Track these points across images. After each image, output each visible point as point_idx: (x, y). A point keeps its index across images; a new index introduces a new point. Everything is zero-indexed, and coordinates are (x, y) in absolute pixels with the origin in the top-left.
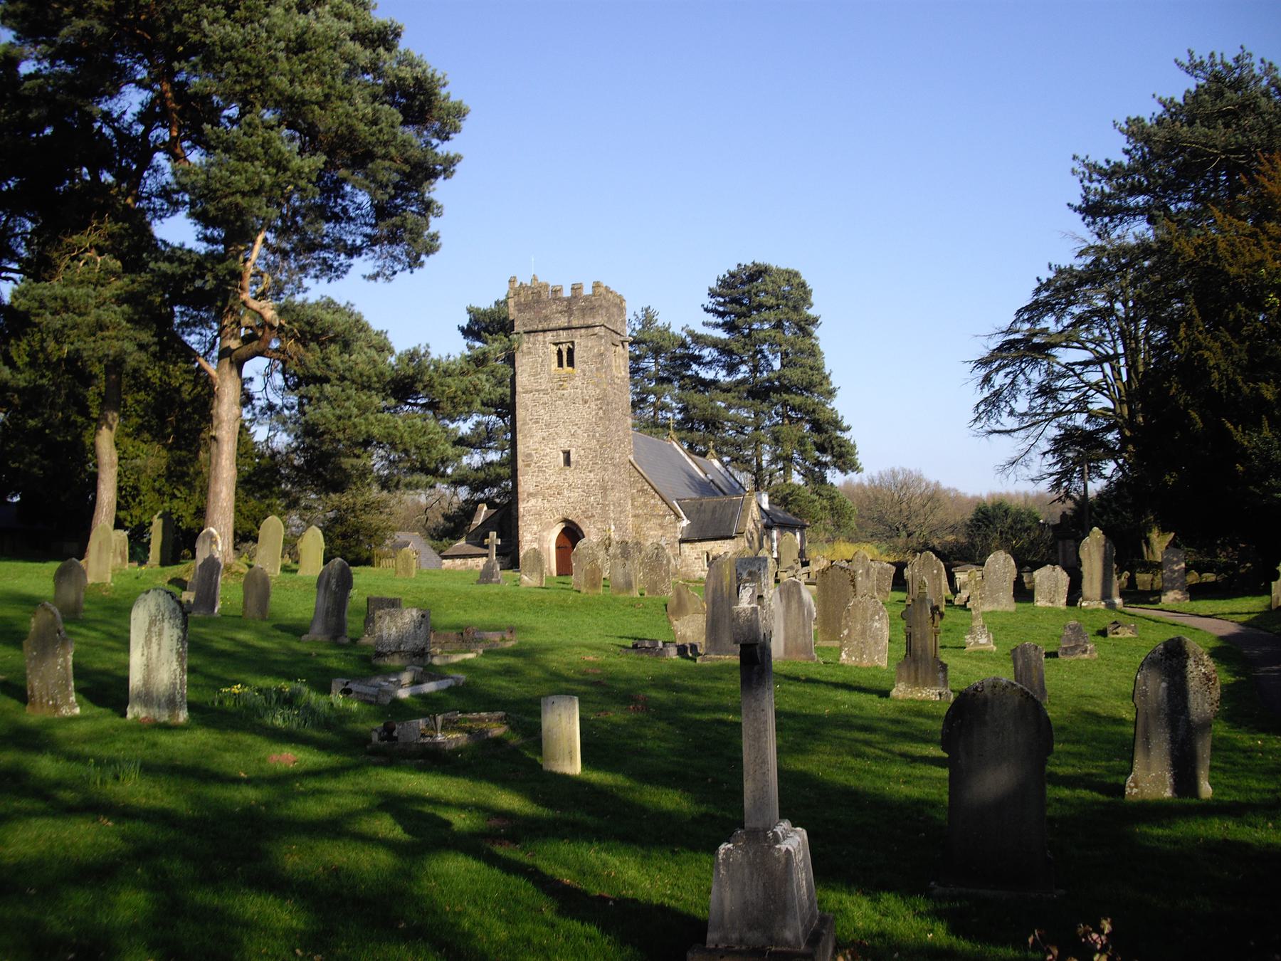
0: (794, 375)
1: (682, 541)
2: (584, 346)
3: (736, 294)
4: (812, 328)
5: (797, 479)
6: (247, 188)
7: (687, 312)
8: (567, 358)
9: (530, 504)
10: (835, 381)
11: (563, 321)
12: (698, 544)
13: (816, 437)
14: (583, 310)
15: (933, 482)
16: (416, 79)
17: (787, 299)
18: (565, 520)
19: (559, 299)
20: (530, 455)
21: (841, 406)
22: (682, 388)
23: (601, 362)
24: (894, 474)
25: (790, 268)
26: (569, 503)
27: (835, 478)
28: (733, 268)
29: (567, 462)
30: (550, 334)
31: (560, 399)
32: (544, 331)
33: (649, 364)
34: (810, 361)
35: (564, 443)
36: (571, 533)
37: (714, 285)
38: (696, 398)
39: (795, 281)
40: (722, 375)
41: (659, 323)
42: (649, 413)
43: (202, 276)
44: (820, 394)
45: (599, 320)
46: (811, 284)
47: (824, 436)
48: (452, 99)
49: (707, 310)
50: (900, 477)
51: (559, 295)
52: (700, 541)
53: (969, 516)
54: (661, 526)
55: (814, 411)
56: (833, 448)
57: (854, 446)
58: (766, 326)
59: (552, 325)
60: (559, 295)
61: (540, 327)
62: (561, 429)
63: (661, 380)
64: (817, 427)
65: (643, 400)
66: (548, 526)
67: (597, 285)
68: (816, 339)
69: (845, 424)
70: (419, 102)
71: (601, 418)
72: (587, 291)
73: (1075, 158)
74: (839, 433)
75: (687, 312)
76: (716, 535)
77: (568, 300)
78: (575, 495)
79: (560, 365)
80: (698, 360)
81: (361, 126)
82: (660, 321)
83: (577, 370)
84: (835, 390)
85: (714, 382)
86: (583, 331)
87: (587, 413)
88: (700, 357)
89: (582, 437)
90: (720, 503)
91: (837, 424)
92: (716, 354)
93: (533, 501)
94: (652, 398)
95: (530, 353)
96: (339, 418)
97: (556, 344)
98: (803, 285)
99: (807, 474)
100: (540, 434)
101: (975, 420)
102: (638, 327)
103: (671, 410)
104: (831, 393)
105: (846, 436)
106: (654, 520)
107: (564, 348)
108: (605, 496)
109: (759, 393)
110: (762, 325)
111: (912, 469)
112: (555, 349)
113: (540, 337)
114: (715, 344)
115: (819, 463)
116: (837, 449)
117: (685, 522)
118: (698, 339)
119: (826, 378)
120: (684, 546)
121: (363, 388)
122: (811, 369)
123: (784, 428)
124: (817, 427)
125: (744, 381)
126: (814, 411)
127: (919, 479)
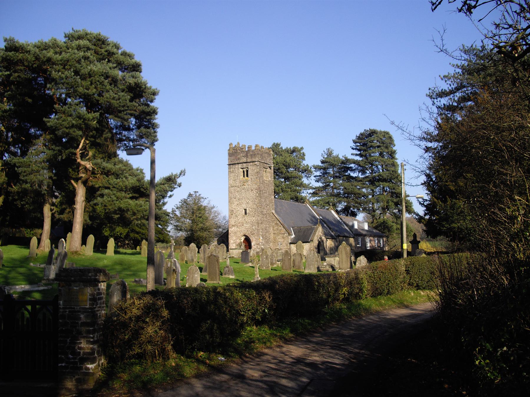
1: (291, 243)
2: (252, 169)
3: (363, 141)
6: (68, 126)
7: (345, 150)
8: (246, 174)
11: (244, 160)
16: (135, 83)
17: (383, 144)
18: (245, 235)
25: (386, 130)
26: (245, 229)
28: (362, 131)
29: (246, 213)
31: (243, 189)
32: (238, 164)
33: (331, 171)
35: (244, 206)
36: (248, 241)
39: (387, 136)
40: (361, 176)
41: (334, 154)
43: (61, 155)
45: (257, 159)
49: (353, 149)
54: (283, 238)
57: (412, 203)
59: (241, 161)
61: (237, 162)
62: (243, 201)
67: (256, 146)
68: (396, 159)
72: (253, 148)
73: (429, 89)
75: (345, 150)
77: (247, 152)
78: (248, 226)
79: (244, 177)
81: (112, 101)
82: (335, 154)
83: (249, 179)
87: (253, 194)
88: (351, 167)
89: (251, 203)
93: (233, 228)
96: (109, 201)
100: (236, 203)
102: (326, 156)
107: (245, 170)
108: (258, 227)
109: (373, 181)
112: (242, 170)
114: (354, 162)
120: (292, 245)
121: (120, 191)
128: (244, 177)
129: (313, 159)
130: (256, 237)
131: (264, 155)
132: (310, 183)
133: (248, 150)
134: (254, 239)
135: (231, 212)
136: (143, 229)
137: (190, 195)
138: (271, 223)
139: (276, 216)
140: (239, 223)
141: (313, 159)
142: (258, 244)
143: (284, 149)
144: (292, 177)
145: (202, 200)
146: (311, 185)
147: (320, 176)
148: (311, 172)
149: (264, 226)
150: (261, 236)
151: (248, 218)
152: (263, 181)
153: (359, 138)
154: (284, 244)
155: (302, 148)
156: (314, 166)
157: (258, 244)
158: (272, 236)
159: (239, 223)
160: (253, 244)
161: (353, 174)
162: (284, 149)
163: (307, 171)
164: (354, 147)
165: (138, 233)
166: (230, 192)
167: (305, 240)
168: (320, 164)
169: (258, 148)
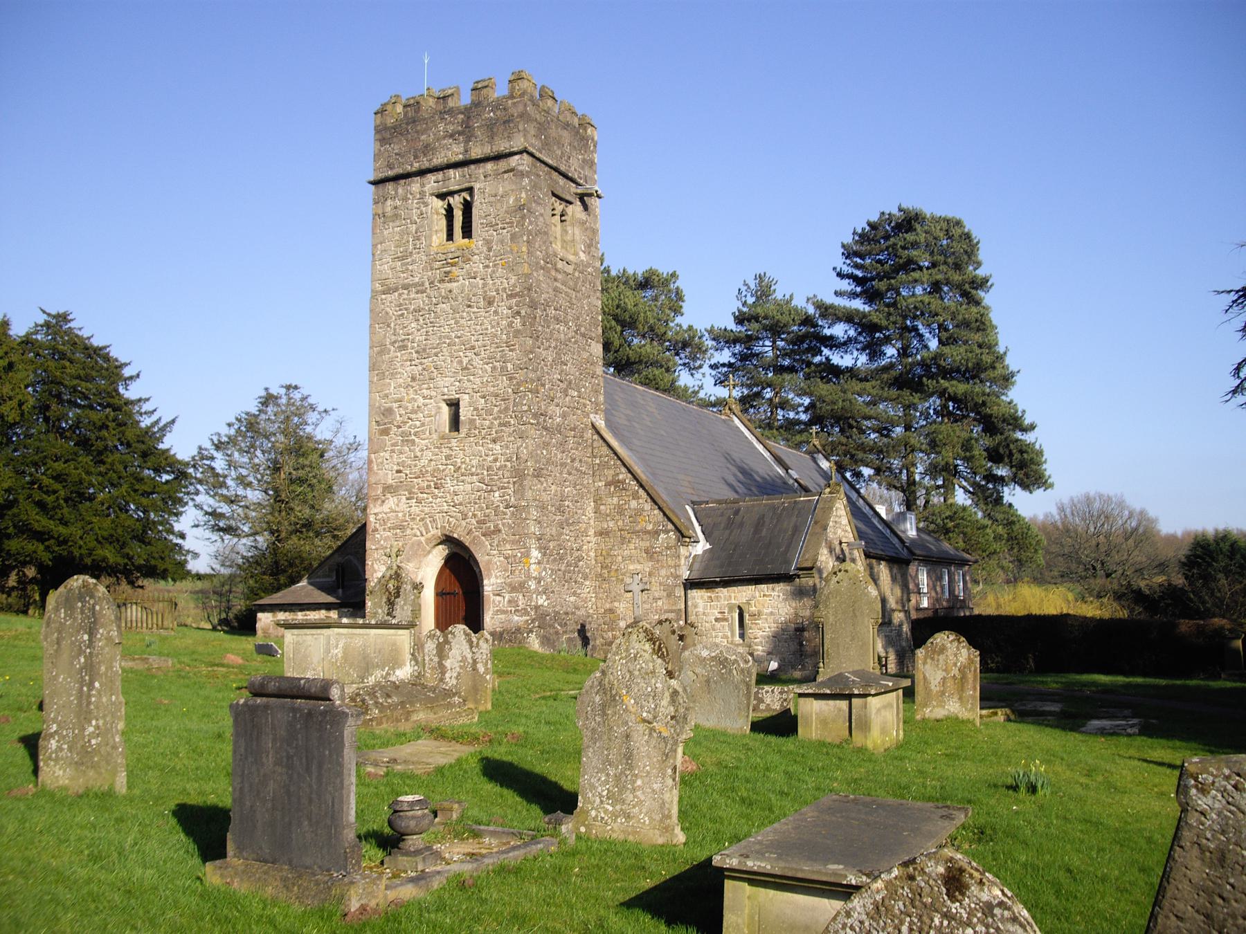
0: (955, 355)
1: (690, 584)
2: (493, 192)
4: (981, 293)
5: (961, 498)
7: (813, 278)
8: (463, 221)
9: (386, 508)
10: (1012, 362)
11: (455, 152)
12: (723, 592)
13: (987, 441)
14: (491, 127)
15: (1138, 510)
18: (448, 540)
19: (451, 112)
20: (389, 411)
21: (1022, 396)
22: (808, 377)
23: (521, 224)
24: (1088, 500)
25: (950, 215)
26: (453, 507)
27: (1014, 496)
28: (875, 218)
29: (455, 423)
30: (431, 178)
32: (422, 173)
33: (766, 348)
34: (978, 337)
35: (448, 385)
37: (848, 239)
38: (823, 389)
39: (956, 232)
41: (779, 295)
42: (763, 411)
44: (993, 381)
45: (518, 143)
46: (976, 235)
47: (998, 438)
48: (794, 303)
49: (841, 275)
50: (1097, 505)
51: (451, 103)
52: (726, 583)
53: (1183, 553)
54: (650, 553)
55: (984, 404)
56: (1011, 455)
57: (1040, 453)
58: (919, 290)
59: (438, 160)
60: (451, 103)
61: (417, 166)
62: (444, 359)
63: (780, 370)
64: (990, 425)
65: (758, 395)
66: (420, 552)
68: (987, 308)
69: (1027, 421)
70: (585, 124)
71: (517, 333)
74: (1019, 435)
75: (813, 278)
76: (757, 571)
77: (467, 111)
79: (450, 236)
80: (831, 342)
82: (779, 293)
83: (477, 243)
84: (1013, 375)
85: (851, 372)
86: (489, 166)
87: (496, 321)
88: (832, 337)
90: (774, 508)
91: (1015, 422)
92: (852, 333)
93: (391, 502)
94: (768, 393)
95: (396, 216)
97: (442, 196)
98: (968, 236)
99: (978, 493)
100: (406, 371)
101: (1234, 392)
102: (751, 300)
103: (794, 408)
104: (1007, 380)
105: (1029, 438)
106: (636, 542)
107: (456, 201)
108: (520, 492)
109: (907, 382)
110: (915, 292)
111: (1111, 494)
112: (439, 205)
113: (415, 185)
115: (991, 477)
116: (1017, 456)
117: (702, 547)
118: (826, 311)
119: (1000, 358)
120: (697, 596)
122: (980, 346)
123: (943, 427)
124: (990, 425)
125: (891, 366)
126: (984, 404)
127: (1121, 504)
128: (450, 236)
129: (708, 308)
130: (508, 549)
131: (553, 131)
132: (701, 387)
133: (476, 104)
134: (498, 560)
135: (383, 420)
136: (65, 524)
137: (268, 399)
138: (588, 480)
139: (615, 443)
140: (421, 475)
141: (708, 308)
142: (519, 588)
143: (614, 273)
144: (640, 362)
145: (312, 417)
146: (702, 395)
147: (730, 365)
148: (701, 350)
149: (548, 490)
150: (533, 544)
151: (466, 450)
152: (550, 261)
153: (863, 238)
154: (656, 591)
155: (674, 275)
156: (710, 332)
157: (519, 588)
158: (590, 544)
159: (421, 475)
160: (490, 585)
161: (843, 360)
162: (614, 273)
163: (688, 346)
164: (847, 270)
165: (40, 536)
166: (378, 318)
167: (770, 569)
168: (731, 325)
169: (524, 85)
